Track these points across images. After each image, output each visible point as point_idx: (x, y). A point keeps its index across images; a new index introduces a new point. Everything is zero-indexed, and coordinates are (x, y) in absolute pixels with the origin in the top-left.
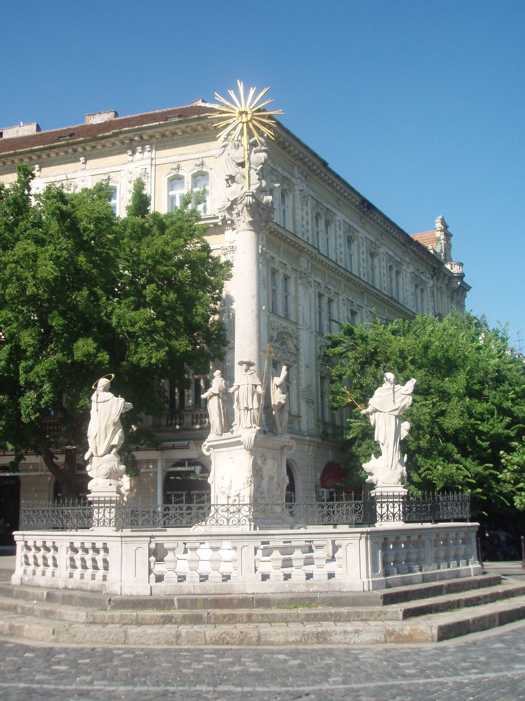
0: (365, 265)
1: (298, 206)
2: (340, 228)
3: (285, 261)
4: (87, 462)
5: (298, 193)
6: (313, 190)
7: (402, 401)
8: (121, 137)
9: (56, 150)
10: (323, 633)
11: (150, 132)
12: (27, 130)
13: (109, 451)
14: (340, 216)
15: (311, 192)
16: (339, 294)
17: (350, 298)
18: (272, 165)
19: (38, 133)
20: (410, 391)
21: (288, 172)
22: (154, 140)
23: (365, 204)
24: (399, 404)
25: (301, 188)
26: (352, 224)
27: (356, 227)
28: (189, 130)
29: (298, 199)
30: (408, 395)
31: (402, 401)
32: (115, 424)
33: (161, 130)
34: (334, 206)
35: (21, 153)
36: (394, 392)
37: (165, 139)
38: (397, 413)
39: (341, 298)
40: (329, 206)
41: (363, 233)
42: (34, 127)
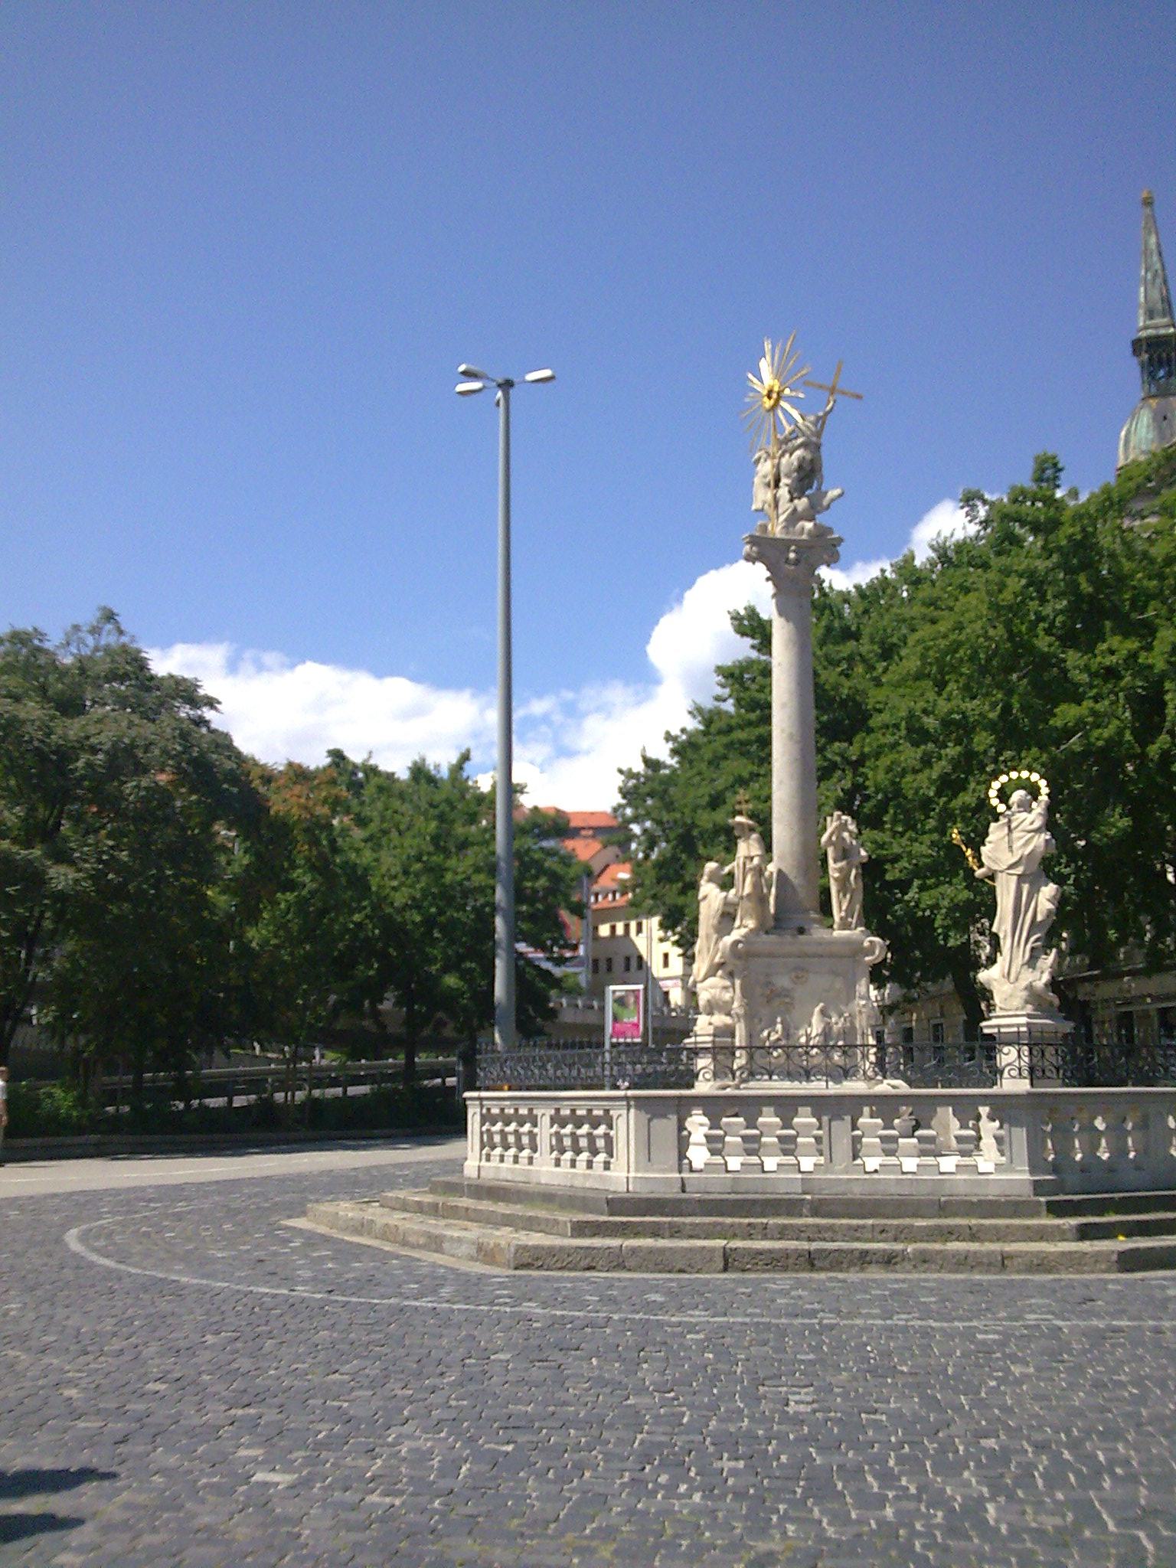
4: (1027, 1002)
13: (711, 972)
30: (1037, 831)
36: (1010, 830)
38: (1020, 870)
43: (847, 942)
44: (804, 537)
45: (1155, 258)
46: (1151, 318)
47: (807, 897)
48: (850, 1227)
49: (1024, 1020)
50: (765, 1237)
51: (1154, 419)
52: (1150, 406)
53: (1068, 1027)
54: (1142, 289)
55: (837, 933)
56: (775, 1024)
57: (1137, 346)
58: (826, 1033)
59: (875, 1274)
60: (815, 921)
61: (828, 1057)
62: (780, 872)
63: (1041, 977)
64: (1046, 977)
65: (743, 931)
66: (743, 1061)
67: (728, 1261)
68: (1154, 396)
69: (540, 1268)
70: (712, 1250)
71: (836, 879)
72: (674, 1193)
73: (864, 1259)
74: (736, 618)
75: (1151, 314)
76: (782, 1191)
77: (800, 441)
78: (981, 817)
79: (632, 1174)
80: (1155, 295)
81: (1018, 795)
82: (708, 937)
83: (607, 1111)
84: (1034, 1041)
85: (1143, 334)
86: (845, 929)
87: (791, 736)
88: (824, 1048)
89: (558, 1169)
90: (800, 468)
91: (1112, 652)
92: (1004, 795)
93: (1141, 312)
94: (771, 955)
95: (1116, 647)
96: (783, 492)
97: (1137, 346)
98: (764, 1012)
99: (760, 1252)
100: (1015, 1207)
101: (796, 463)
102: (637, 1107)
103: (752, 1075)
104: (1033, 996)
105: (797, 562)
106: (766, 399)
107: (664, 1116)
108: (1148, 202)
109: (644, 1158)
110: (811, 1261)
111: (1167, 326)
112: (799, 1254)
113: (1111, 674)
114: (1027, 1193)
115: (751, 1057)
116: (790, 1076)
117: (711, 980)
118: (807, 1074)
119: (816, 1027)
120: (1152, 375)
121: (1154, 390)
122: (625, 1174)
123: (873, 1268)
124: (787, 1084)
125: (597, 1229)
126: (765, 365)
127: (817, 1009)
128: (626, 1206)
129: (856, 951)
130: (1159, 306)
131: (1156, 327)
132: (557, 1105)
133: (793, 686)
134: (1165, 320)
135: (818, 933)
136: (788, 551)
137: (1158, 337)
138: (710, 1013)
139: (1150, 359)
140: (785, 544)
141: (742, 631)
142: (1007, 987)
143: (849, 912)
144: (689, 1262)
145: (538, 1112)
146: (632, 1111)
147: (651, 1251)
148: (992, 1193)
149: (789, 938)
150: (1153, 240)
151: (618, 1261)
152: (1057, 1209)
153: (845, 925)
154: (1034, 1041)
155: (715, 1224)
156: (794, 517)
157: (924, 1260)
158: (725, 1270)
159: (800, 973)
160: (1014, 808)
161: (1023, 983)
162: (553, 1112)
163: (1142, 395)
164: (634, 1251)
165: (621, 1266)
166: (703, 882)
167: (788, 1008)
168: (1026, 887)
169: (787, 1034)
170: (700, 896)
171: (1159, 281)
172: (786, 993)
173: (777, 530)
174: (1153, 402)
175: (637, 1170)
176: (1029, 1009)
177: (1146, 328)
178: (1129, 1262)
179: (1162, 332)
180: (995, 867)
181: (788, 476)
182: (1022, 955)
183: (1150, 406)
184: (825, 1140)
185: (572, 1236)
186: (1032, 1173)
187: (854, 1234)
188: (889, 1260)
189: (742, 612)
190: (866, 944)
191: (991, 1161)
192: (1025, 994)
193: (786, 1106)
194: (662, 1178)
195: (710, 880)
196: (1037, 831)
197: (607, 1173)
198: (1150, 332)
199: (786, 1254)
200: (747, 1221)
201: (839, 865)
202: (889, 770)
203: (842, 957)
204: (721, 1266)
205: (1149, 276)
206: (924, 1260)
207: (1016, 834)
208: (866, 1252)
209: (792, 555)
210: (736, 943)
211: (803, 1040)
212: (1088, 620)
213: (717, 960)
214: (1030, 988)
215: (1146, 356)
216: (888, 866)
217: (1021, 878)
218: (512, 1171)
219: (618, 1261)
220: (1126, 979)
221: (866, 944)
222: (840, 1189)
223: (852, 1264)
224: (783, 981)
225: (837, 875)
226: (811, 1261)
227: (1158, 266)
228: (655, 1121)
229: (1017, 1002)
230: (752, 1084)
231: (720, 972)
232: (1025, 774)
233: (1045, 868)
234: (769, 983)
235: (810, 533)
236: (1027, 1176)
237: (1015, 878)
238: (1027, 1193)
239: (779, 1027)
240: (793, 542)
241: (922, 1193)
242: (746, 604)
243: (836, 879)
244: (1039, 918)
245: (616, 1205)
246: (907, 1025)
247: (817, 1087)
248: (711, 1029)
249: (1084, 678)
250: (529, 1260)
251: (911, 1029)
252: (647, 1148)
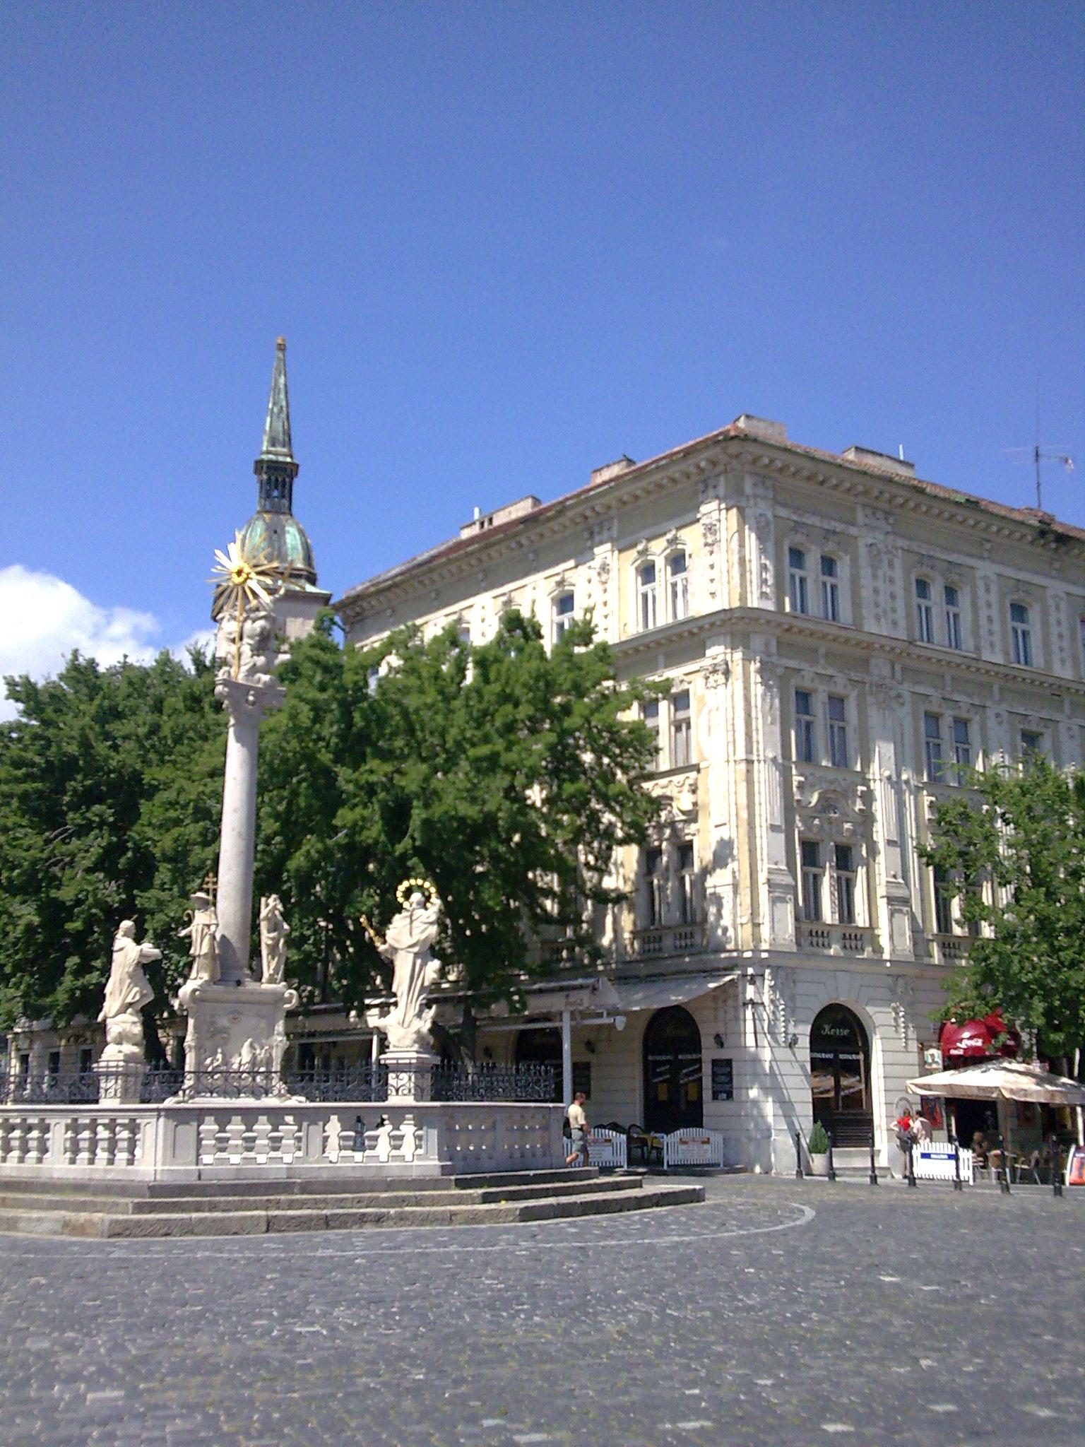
0: (1066, 644)
1: (866, 572)
2: (988, 590)
3: (830, 671)
4: (415, 1042)
5: (863, 551)
6: (911, 539)
7: (423, 932)
8: (570, 514)
9: (497, 547)
10: (12, 1218)
11: (604, 500)
12: (523, 509)
13: (124, 1008)
14: (985, 569)
15: (900, 542)
16: (984, 707)
17: (1021, 710)
18: (795, 518)
19: (536, 509)
20: (433, 918)
21: (841, 520)
22: (613, 512)
23: (1051, 537)
24: (418, 935)
25: (870, 541)
26: (1022, 576)
27: (1036, 579)
28: (651, 487)
29: (864, 561)
30: (431, 923)
31: (423, 932)
32: (131, 976)
33: (617, 494)
34: (971, 556)
35: (457, 559)
36: (412, 922)
37: (627, 507)
38: (416, 949)
39: (990, 713)
40: (954, 558)
41: (1056, 588)
42: (529, 502)
43: (274, 993)
44: (260, 686)
45: (282, 396)
46: (273, 445)
47: (242, 954)
48: (337, 1200)
49: (415, 1055)
50: (278, 1208)
51: (267, 529)
52: (264, 519)
53: (437, 1060)
54: (268, 419)
55: (265, 986)
56: (216, 1053)
57: (259, 465)
58: (253, 1062)
59: (369, 1229)
60: (247, 976)
61: (254, 1079)
62: (223, 937)
63: (425, 1025)
64: (428, 1025)
65: (199, 982)
66: (191, 1083)
67: (270, 1225)
68: (267, 512)
69: (128, 1236)
70: (259, 1217)
71: (268, 945)
72: (193, 1180)
73: (362, 1219)
74: (11, 683)
75: (273, 442)
76: (272, 1177)
77: (263, 613)
78: (390, 909)
79: (159, 1167)
80: (279, 427)
81: (416, 897)
82: (121, 981)
83: (43, 1120)
84: (418, 1069)
85: (265, 457)
86: (271, 981)
87: (240, 834)
88: (253, 1073)
89: (73, 1166)
90: (261, 634)
91: (372, 772)
92: (408, 893)
93: (266, 438)
94: (216, 1001)
95: (376, 770)
96: (246, 650)
97: (259, 465)
98: (208, 1044)
99: (293, 1218)
100: (434, 1184)
101: (258, 630)
102: (167, 1117)
103: (198, 1093)
104: (420, 1039)
105: (253, 703)
106: (235, 576)
107: (188, 1123)
108: (282, 348)
109: (169, 1153)
110: (327, 1222)
111: (286, 455)
112: (319, 1217)
113: (371, 790)
114: (437, 1173)
115: (198, 1079)
116: (225, 1094)
117: (122, 1017)
118: (238, 1093)
119: (246, 1056)
120: (268, 496)
121: (268, 507)
122: (152, 1168)
123: (367, 1225)
124: (222, 1100)
125: (153, 1208)
126: (234, 549)
127: (247, 1044)
128: (162, 1194)
129: (279, 999)
130: (281, 437)
131: (276, 454)
132: (75, 1115)
133: (244, 796)
134: (285, 450)
135: (250, 985)
136: (248, 694)
137: (276, 462)
138: (120, 1043)
139: (269, 479)
140: (246, 689)
141: (14, 695)
142: (402, 1031)
143: (276, 970)
144: (241, 1228)
145: (51, 1121)
146: (162, 1120)
147: (214, 1220)
148: (415, 1174)
149: (232, 989)
150: (282, 380)
151: (167, 1230)
152: (461, 1184)
153: (272, 980)
154: (418, 1069)
155: (242, 1202)
156: (254, 670)
157: (402, 1218)
158: (267, 1231)
159: (236, 1016)
160: (414, 906)
161: (414, 1028)
162: (69, 1121)
163: (259, 509)
164: (201, 1220)
165: (192, 1232)
166: (118, 936)
167: (225, 1042)
168: (419, 962)
169: (226, 1062)
170: (116, 948)
171: (283, 416)
172: (225, 1030)
173: (241, 679)
174: (266, 516)
175: (164, 1164)
176: (416, 1047)
177: (268, 452)
178: (527, 1215)
179: (281, 459)
180: (396, 945)
181: (250, 637)
182: (414, 1009)
183: (264, 519)
184: (304, 1140)
185: (870, 1141)
186: (440, 1160)
187: (340, 1203)
188: (379, 1220)
189: (17, 679)
190: (286, 995)
191: (405, 1150)
192: (414, 1036)
193: (223, 1116)
194: (183, 1170)
195: (125, 935)
196: (431, 923)
197: (130, 1167)
198: (271, 457)
199: (310, 1218)
200: (265, 1198)
201: (272, 935)
202: (176, 840)
203: (265, 1004)
204: (264, 1229)
205: (276, 410)
206: (402, 1218)
207: (414, 924)
208: (364, 1215)
209: (251, 698)
210: (194, 991)
211: (235, 1067)
212: (354, 747)
213: (129, 1000)
214: (418, 1032)
215: (265, 477)
216: (148, 917)
217: (416, 955)
218: (19, 1169)
219: (167, 1230)
220: (300, 1018)
221: (286, 995)
222: (314, 1174)
223: (355, 1223)
224: (223, 1022)
225: (270, 942)
226: (327, 1222)
227: (284, 404)
228: (180, 1127)
229: (408, 1042)
230: (197, 1100)
231: (130, 1010)
232: (420, 882)
233: (433, 950)
234: (213, 1023)
235: (265, 683)
236: (437, 1163)
237: (411, 956)
238: (437, 1173)
239: (219, 1056)
240: (251, 688)
241: (369, 1175)
242: (24, 673)
243: (268, 945)
244: (426, 984)
245: (155, 1190)
246: (55, 1050)
247: (246, 1101)
248: (121, 1057)
249: (351, 787)
250: (119, 1231)
251: (57, 1054)
252: (173, 1148)
